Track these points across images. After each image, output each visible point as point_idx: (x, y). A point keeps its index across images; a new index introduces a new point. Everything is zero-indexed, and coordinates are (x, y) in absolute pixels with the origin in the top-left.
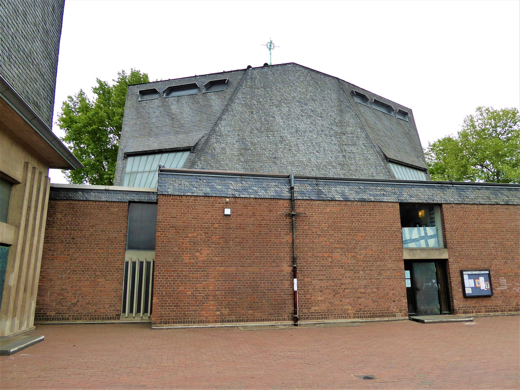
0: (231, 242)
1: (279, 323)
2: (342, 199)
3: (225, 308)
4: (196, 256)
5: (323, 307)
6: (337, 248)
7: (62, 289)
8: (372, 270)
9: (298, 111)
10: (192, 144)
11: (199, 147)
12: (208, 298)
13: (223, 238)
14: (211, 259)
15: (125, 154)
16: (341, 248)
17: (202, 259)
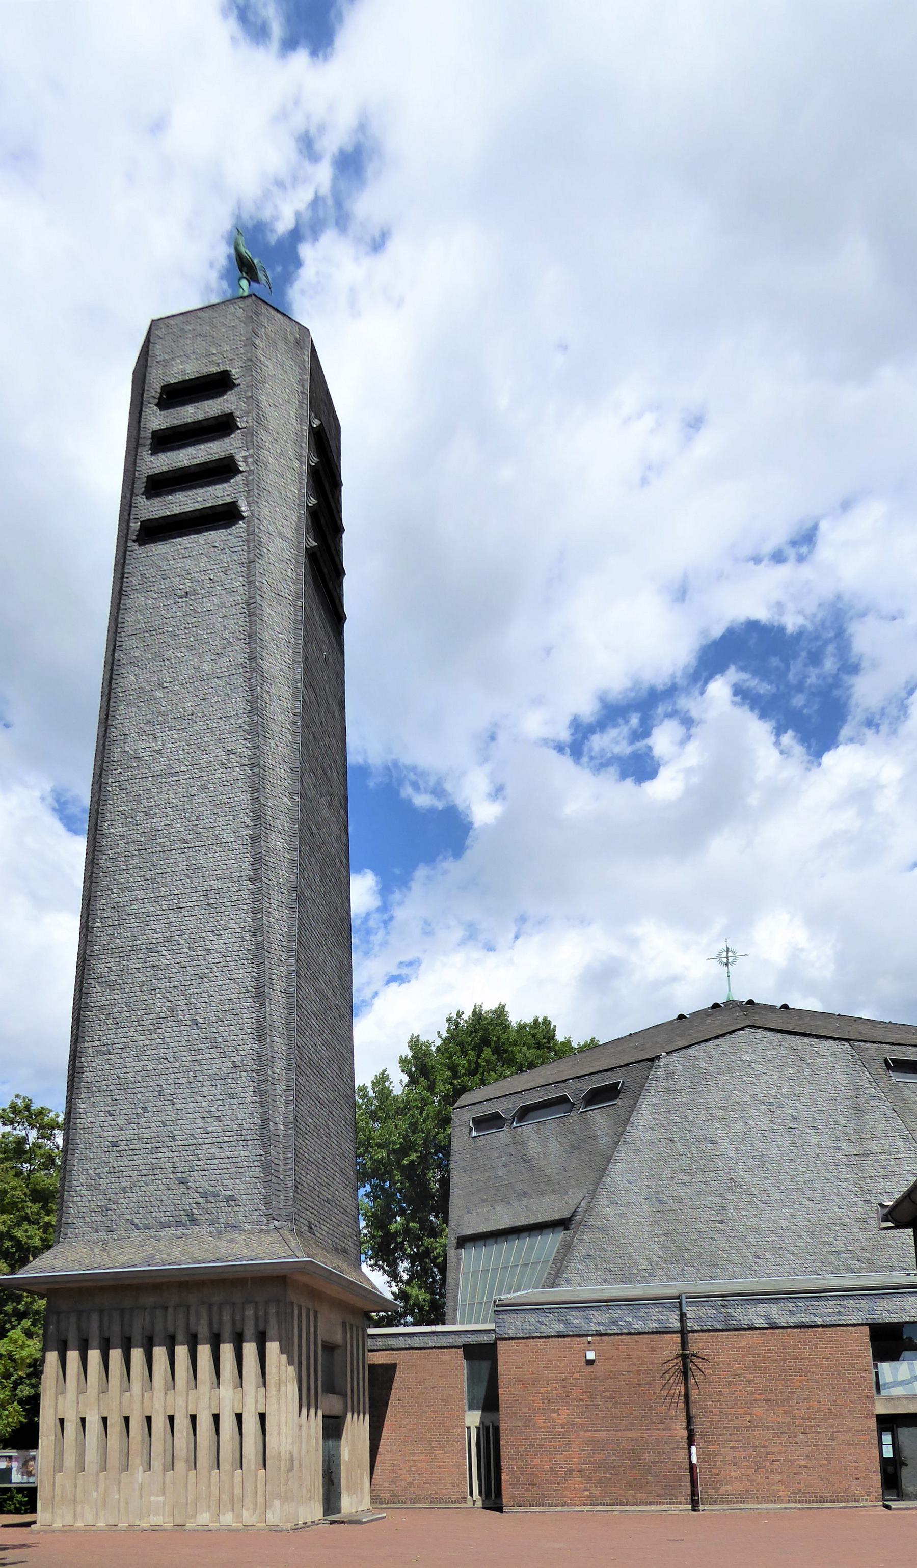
1: (673, 1507)
2: (767, 1326)
3: (596, 1486)
5: (739, 1486)
6: (760, 1400)
7: (395, 1466)
8: (819, 1432)
9: (764, 1123)
10: (566, 1215)
11: (578, 1218)
15: (459, 1238)
16: (767, 1401)
17: (560, 1422)
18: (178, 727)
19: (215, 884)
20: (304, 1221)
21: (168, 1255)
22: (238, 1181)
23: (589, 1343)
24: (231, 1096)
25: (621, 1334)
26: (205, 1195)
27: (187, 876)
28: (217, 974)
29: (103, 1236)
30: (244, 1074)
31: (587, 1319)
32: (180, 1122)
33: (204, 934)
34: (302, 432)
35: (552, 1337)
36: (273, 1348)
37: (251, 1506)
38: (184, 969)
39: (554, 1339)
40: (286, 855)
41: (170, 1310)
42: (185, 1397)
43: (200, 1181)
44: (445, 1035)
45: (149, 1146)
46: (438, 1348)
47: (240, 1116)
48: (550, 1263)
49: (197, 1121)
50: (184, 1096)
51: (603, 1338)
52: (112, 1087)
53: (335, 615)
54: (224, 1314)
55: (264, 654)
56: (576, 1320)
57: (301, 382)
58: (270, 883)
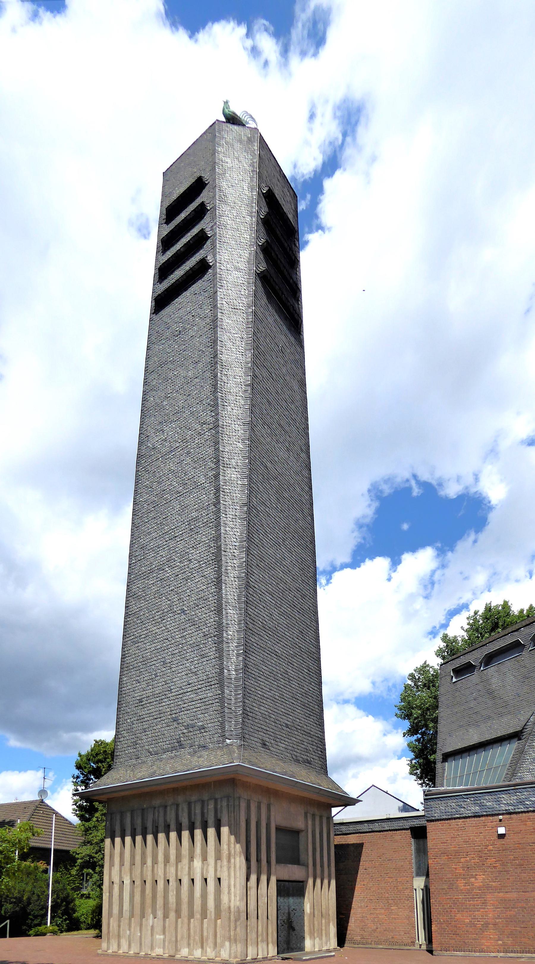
0: (509, 864)
4: (471, 882)
10: (519, 729)
12: (488, 927)
13: (499, 861)
14: (488, 884)
15: (443, 755)
18: (175, 419)
19: (194, 514)
20: (256, 739)
21: (164, 770)
22: (206, 715)
23: (500, 820)
24: (203, 656)
25: (528, 812)
26: (187, 727)
27: (179, 514)
28: (195, 575)
29: (134, 762)
30: (210, 639)
31: (499, 802)
32: (174, 680)
33: (188, 551)
34: (252, 197)
35: (469, 817)
36: (225, 830)
37: (212, 945)
38: (177, 577)
39: (471, 819)
40: (239, 482)
41: (168, 808)
42: (175, 867)
43: (185, 718)
44: (466, 627)
45: (158, 699)
46: (392, 830)
47: (207, 669)
48: (508, 765)
49: (184, 677)
50: (177, 662)
51: (512, 816)
52: (140, 664)
53: (294, 322)
54: (197, 808)
55: (223, 351)
56: (489, 802)
57: (252, 165)
58: (227, 503)
